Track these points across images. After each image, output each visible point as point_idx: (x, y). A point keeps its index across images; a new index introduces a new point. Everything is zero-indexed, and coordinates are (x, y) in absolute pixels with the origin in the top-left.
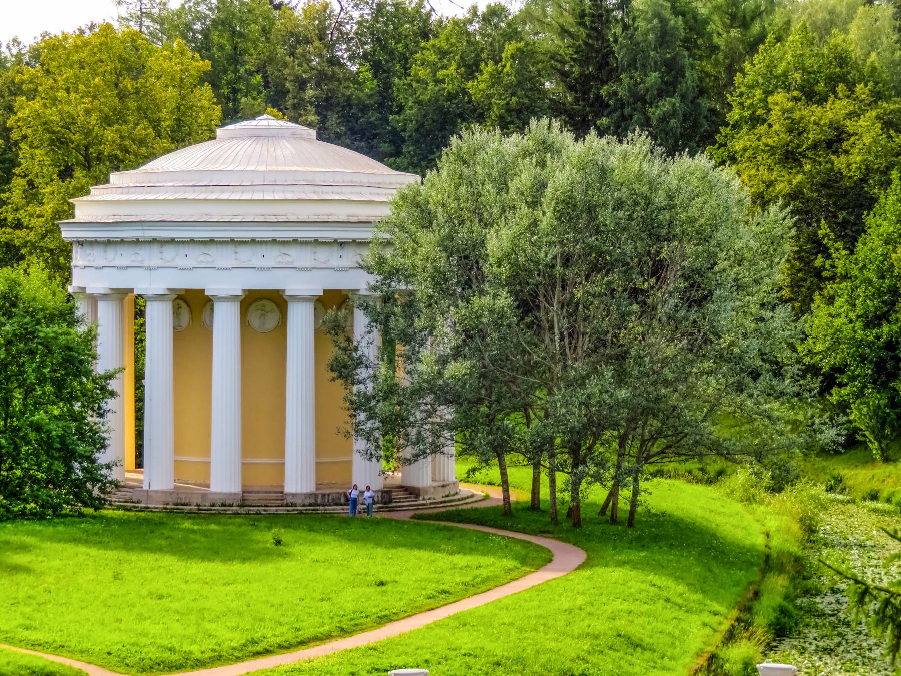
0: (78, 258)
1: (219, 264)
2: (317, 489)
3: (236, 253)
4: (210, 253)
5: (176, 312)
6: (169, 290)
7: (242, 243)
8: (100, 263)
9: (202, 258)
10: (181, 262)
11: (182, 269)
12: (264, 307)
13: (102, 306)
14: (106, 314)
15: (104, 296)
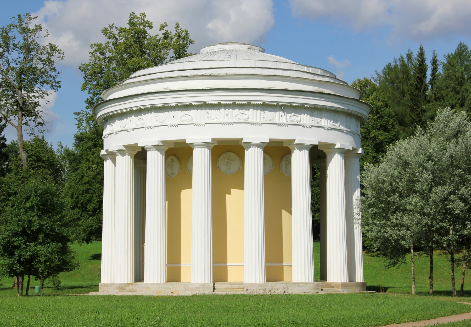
12: (278, 153)
14: (125, 164)
15: (121, 152)
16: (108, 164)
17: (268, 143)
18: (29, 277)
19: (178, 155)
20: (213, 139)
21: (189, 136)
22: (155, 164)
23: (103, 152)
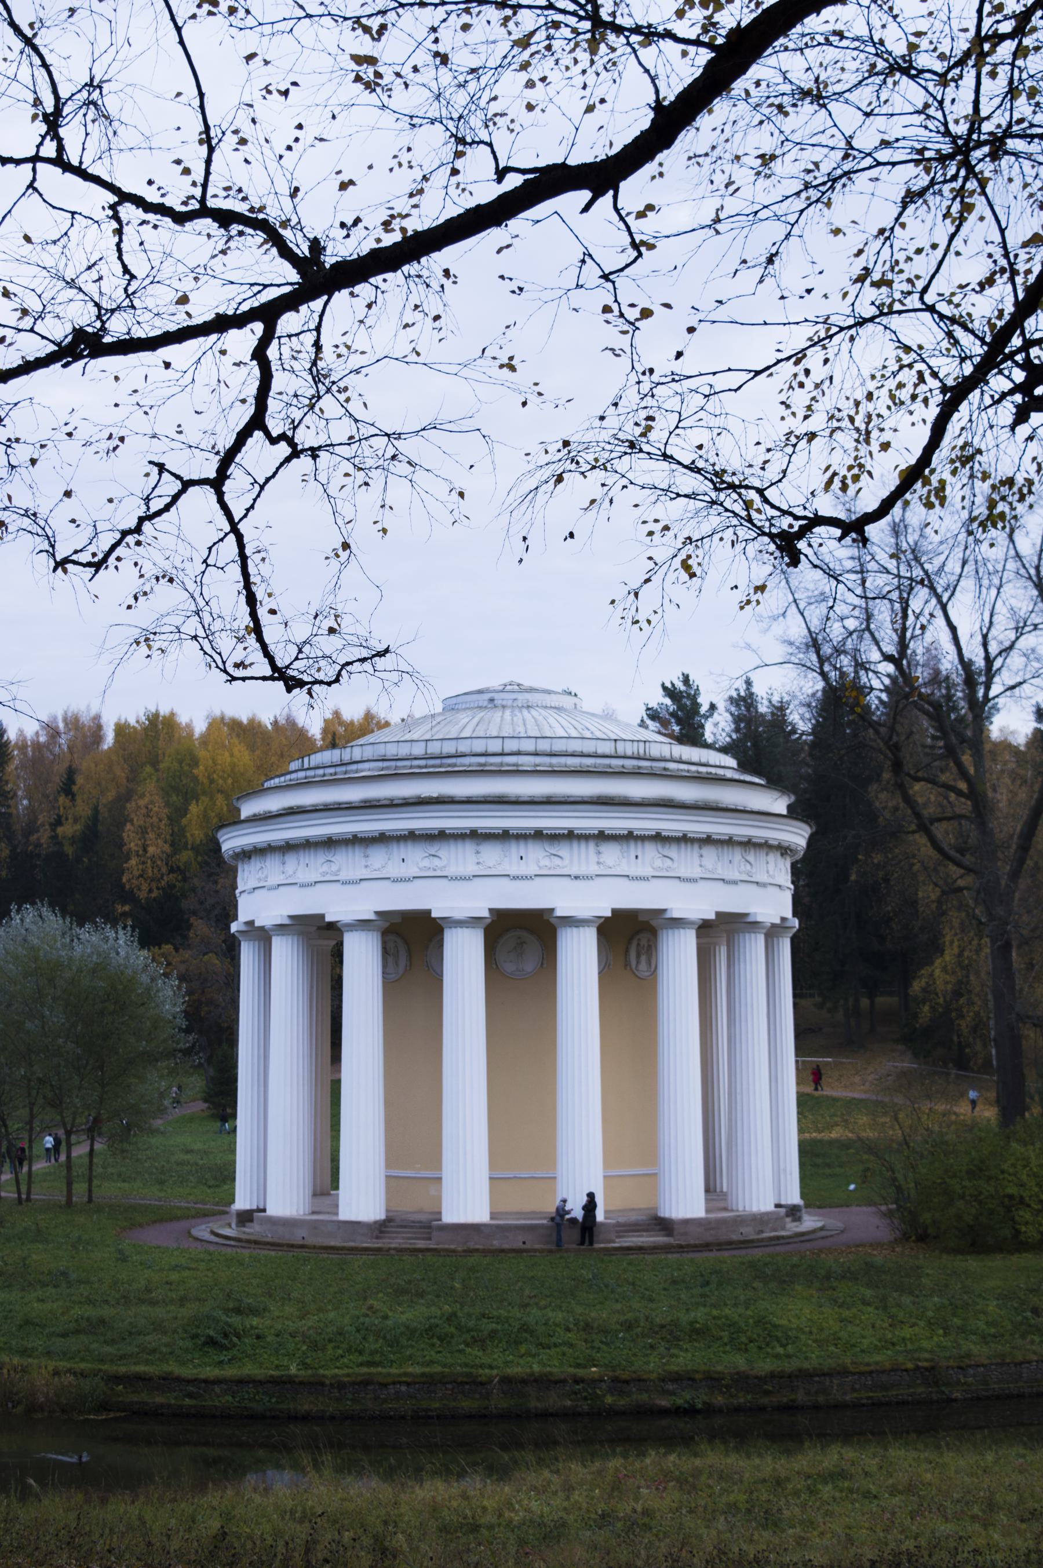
0: (247, 877)
1: (452, 870)
2: (707, 1211)
3: (478, 852)
4: (560, 853)
5: (387, 953)
6: (377, 913)
7: (643, 839)
9: (426, 863)
10: (395, 869)
11: (396, 881)
12: (629, 937)
14: (285, 954)
15: (281, 928)
16: (248, 956)
17: (607, 918)
18: (81, 163)
19: (414, 940)
20: (614, 911)
21: (441, 902)
22: (362, 963)
23: (234, 927)
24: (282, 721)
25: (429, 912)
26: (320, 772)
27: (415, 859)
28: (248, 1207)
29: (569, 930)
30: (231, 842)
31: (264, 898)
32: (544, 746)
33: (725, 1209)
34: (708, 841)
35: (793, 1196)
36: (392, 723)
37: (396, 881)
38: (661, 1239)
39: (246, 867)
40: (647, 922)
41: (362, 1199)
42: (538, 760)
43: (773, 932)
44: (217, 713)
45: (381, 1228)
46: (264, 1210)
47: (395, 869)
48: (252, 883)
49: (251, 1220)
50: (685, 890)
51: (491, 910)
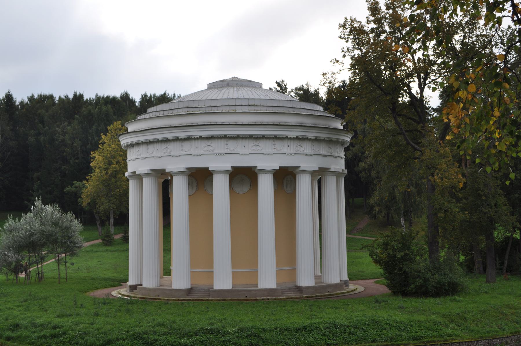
0: (131, 154)
2: (315, 283)
4: (259, 144)
5: (190, 184)
6: (187, 168)
8: (271, 151)
10: (240, 150)
11: (194, 155)
13: (146, 180)
15: (147, 174)
16: (132, 185)
20: (280, 167)
22: (180, 189)
23: (126, 174)
24: (63, 97)
25: (208, 168)
26: (162, 113)
27: (202, 147)
28: (134, 284)
29: (304, 175)
30: (124, 141)
31: (137, 163)
32: (251, 103)
33: (321, 282)
34: (276, 138)
35: (346, 278)
36: (264, 87)
37: (194, 155)
38: (298, 295)
39: (131, 150)
40: (292, 172)
41: (180, 280)
42: (250, 108)
43: (338, 175)
44: (39, 94)
45: (189, 291)
46: (141, 285)
47: (285, 150)
48: (134, 157)
49: (136, 289)
50: (304, 158)
51: (232, 167)
